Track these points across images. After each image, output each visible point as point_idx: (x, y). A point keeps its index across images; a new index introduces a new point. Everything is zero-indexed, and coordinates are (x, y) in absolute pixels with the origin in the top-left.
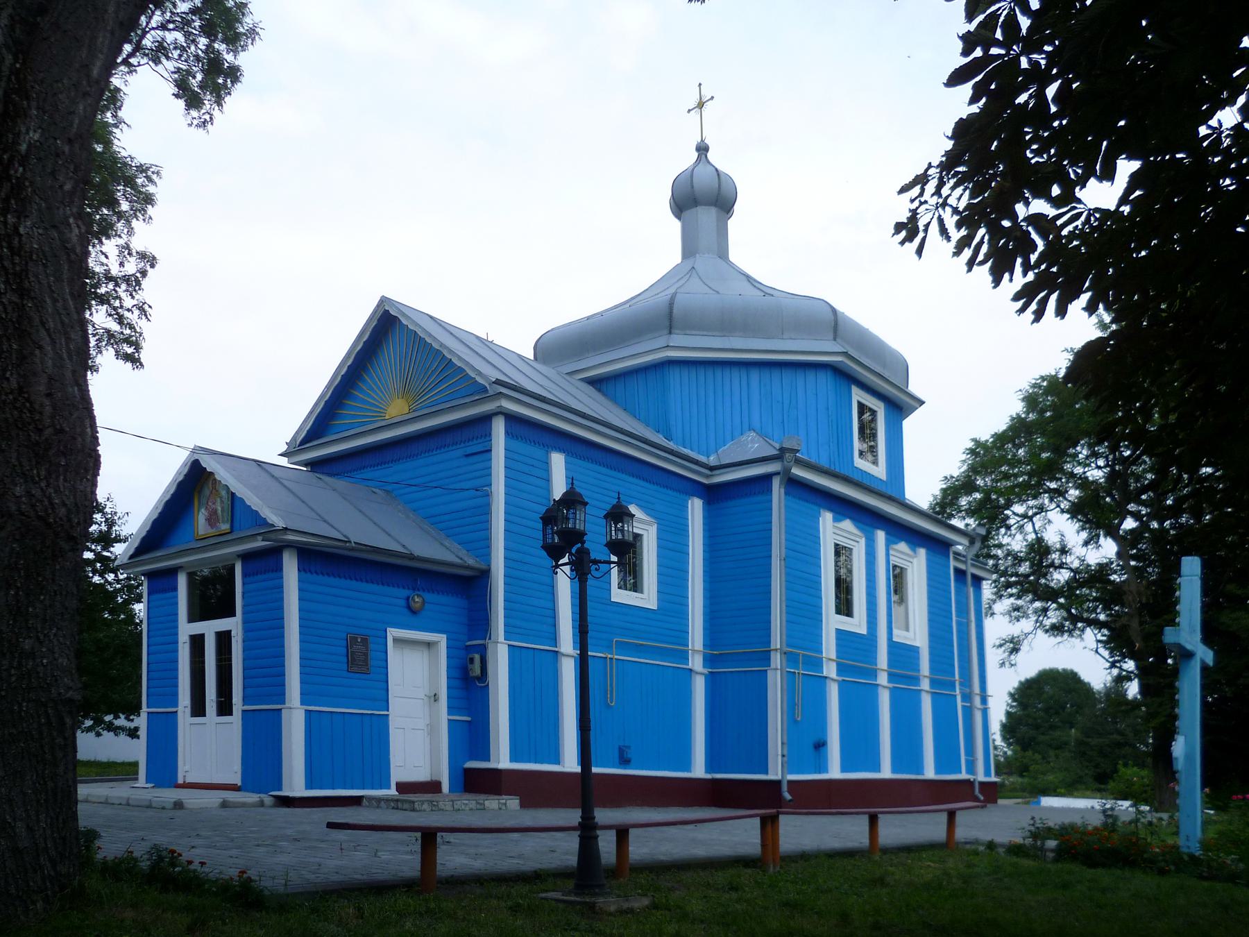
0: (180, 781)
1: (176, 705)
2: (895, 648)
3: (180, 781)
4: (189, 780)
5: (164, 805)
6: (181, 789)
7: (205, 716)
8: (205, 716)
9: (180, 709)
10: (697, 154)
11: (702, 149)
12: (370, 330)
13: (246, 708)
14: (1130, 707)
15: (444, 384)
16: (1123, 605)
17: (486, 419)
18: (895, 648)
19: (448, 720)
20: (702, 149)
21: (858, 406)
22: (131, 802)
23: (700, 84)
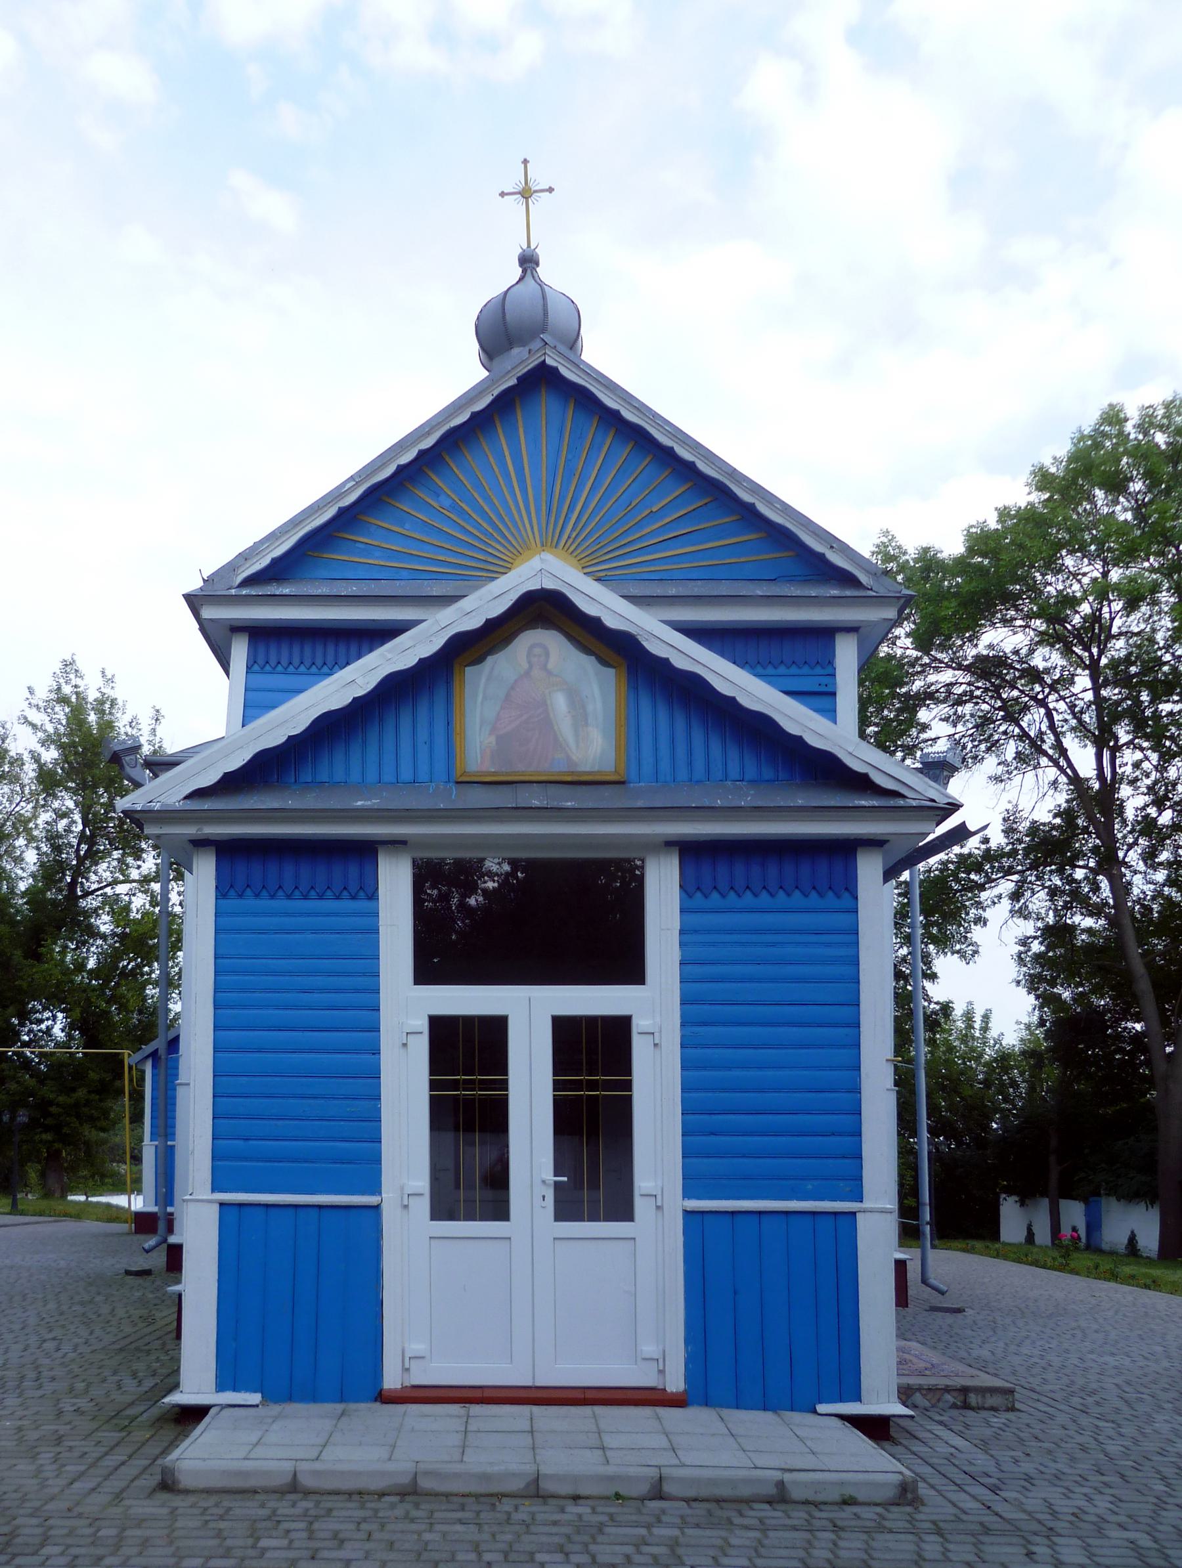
0: (392, 1380)
1: (376, 1189)
2: (54, 1048)
3: (392, 1380)
4: (421, 1376)
5: (850, 1491)
6: (394, 1405)
7: (432, 1219)
8: (432, 1219)
9: (389, 1198)
10: (520, 270)
11: (528, 261)
12: (496, 393)
13: (694, 1204)
14: (98, 1124)
15: (682, 547)
16: (67, 1004)
17: (826, 634)
18: (54, 1048)
19: (687, 1213)
20: (528, 261)
21: (255, 718)
22: (668, 1488)
23: (525, 162)
